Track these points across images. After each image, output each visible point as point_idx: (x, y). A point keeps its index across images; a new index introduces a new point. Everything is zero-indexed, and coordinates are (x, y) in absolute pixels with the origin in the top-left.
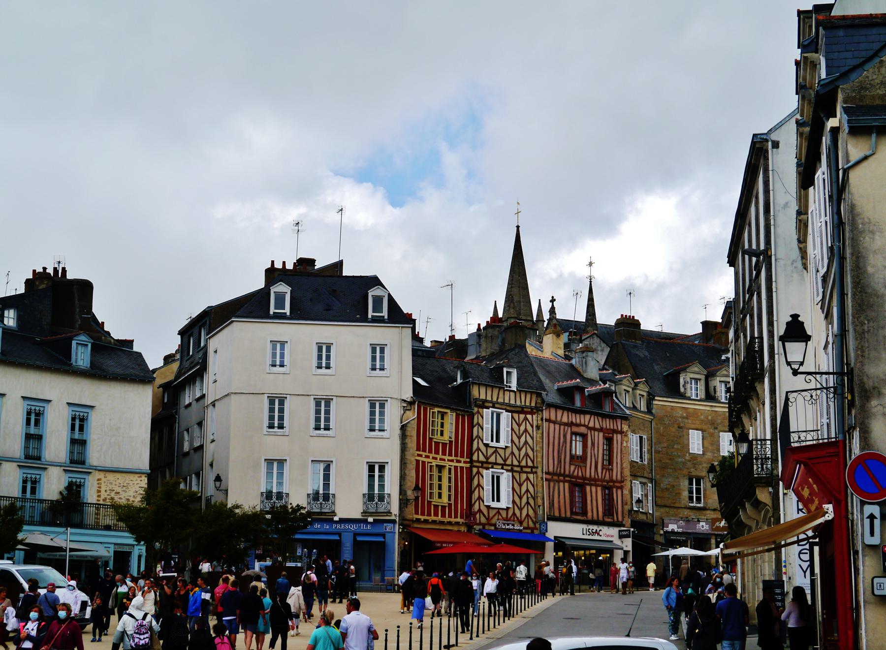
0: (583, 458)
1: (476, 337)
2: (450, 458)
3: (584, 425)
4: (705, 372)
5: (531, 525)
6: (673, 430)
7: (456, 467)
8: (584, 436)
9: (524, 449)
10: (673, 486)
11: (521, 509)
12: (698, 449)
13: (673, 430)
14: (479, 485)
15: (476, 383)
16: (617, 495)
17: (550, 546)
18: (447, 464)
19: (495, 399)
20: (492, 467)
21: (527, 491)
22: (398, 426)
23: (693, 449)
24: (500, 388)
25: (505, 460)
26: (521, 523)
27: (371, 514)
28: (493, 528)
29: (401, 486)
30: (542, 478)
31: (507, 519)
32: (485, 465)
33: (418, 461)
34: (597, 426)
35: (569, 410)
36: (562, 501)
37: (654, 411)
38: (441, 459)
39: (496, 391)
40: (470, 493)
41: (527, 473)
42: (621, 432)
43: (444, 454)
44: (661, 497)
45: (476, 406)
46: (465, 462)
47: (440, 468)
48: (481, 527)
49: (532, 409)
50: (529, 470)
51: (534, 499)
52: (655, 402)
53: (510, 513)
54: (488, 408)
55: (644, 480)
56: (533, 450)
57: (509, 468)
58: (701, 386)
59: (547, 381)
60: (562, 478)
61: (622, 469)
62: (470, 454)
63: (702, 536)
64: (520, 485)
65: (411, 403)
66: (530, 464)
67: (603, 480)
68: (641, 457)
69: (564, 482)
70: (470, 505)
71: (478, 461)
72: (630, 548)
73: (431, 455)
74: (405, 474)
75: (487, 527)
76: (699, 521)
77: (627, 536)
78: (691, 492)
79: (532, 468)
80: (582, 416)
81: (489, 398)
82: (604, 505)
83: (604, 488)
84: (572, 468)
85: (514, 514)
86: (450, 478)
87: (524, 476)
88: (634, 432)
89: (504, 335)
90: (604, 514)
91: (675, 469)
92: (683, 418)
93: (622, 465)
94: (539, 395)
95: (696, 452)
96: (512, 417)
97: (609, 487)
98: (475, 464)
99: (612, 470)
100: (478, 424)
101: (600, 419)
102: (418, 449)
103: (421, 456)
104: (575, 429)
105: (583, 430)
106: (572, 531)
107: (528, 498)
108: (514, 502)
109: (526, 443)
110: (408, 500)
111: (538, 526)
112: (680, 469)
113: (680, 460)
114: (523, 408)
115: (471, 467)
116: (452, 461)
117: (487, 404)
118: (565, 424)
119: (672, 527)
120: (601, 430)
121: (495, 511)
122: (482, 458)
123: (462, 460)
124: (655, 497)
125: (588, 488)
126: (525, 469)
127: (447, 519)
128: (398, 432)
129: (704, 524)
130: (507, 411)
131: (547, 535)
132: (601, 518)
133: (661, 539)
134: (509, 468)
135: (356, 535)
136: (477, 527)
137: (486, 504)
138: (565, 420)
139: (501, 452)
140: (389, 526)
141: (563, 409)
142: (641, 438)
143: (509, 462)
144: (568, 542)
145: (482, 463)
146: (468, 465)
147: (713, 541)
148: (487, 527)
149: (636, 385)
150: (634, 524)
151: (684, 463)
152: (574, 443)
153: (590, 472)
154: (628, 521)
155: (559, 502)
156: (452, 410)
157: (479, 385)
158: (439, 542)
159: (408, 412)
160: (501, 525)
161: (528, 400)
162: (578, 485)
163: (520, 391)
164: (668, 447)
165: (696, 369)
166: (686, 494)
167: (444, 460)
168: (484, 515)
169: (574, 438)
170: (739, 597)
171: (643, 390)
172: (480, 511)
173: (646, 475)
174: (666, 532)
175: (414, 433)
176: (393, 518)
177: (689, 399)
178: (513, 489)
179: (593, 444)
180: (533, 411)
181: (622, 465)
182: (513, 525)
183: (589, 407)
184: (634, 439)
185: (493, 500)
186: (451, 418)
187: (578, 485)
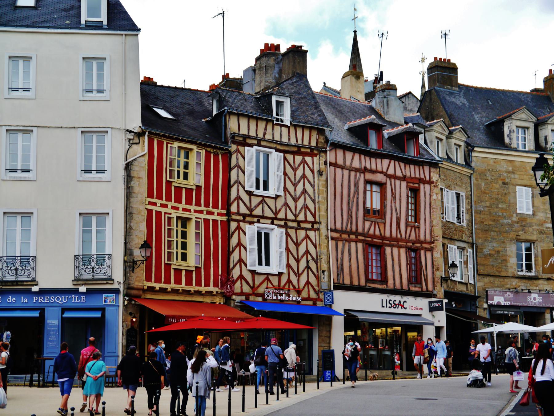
0: (381, 214)
1: (251, 72)
2: (198, 208)
3: (382, 172)
4: (534, 119)
5: (313, 295)
6: (497, 186)
7: (206, 221)
8: (381, 185)
9: (302, 200)
10: (498, 252)
11: (298, 275)
12: (528, 209)
13: (497, 186)
14: (239, 244)
15: (234, 114)
16: (426, 258)
17: (338, 322)
18: (194, 216)
19: (260, 135)
20: (258, 222)
21: (307, 252)
22: (122, 164)
23: (521, 208)
24: (268, 121)
25: (276, 213)
26: (299, 292)
27: (85, 282)
28: (260, 299)
29: (126, 244)
30: (327, 237)
31: (279, 288)
32: (248, 219)
33: (150, 212)
34: (399, 174)
35: (361, 152)
36: (354, 266)
37: (473, 164)
38: (184, 210)
39: (262, 125)
40: (227, 254)
41: (306, 229)
42: (430, 182)
43: (189, 202)
44: (484, 265)
45: (234, 142)
46: (219, 214)
47: (184, 221)
48: (243, 298)
49: (312, 149)
50: (309, 226)
51: (316, 263)
52: (474, 154)
53: (284, 279)
54: (251, 146)
55: (462, 245)
56: (314, 201)
57: (282, 223)
58: (530, 135)
59: (336, 120)
60: (353, 237)
61: (432, 226)
62: (227, 204)
63: (535, 310)
64: (297, 245)
65: (140, 135)
66: (310, 218)
67: (408, 241)
68: (459, 218)
69: (356, 241)
70: (227, 270)
71: (238, 214)
72: (443, 323)
73: (170, 204)
74: (131, 228)
75: (252, 298)
76: (530, 292)
77: (441, 309)
78: (519, 257)
79: (313, 223)
80: (379, 161)
81: (252, 133)
82: (409, 270)
83: (409, 250)
84: (367, 224)
85: (289, 281)
86: (197, 234)
87: (302, 234)
88: (449, 187)
89: (281, 65)
90: (410, 282)
91: (500, 232)
92: (509, 172)
93: (431, 222)
94: (321, 132)
95: (525, 212)
96: (285, 159)
97: (415, 249)
98: (234, 217)
99: (419, 228)
100: (238, 166)
101: (402, 165)
102: (150, 195)
103: (155, 204)
104: (369, 176)
105: (380, 178)
106: (369, 303)
107: (308, 261)
108: (288, 266)
109: (304, 191)
110: (134, 262)
111: (321, 296)
112: (506, 232)
113: (505, 221)
114: (299, 147)
115: (229, 221)
116: (201, 212)
117: (249, 141)
118: (357, 170)
119: (498, 300)
120: (404, 178)
121: (262, 278)
122: (243, 210)
123: (216, 211)
124: (477, 264)
125: (388, 250)
126: (303, 225)
127: (194, 288)
128: (122, 173)
129: (536, 295)
130: (277, 150)
131: (335, 307)
132: (405, 286)
133: (485, 314)
134: (282, 223)
135: (64, 310)
136: (238, 299)
137: (249, 268)
138: (356, 164)
139: (271, 202)
140: (111, 297)
141: (354, 150)
142: (458, 195)
143: (281, 215)
144: (360, 316)
145: (244, 216)
146: (224, 218)
147: (548, 316)
148: (252, 298)
149: (451, 132)
150: (447, 294)
151: (511, 225)
152: (369, 193)
153: (389, 229)
154: (440, 291)
155: (350, 266)
156: (200, 145)
157: (239, 115)
158: (173, 317)
159: (134, 146)
160: (271, 295)
161: (308, 139)
162: (376, 245)
163: (295, 126)
164: (490, 207)
165: (523, 116)
166: (513, 261)
167: (189, 211)
168: (248, 283)
169: (368, 187)
170: (5, 367)
171: (459, 138)
172: (241, 277)
173: (465, 239)
174: (490, 306)
175: (144, 174)
176: (116, 286)
177: (516, 150)
178: (288, 250)
179: (393, 196)
180: (313, 152)
181: (431, 222)
182: (288, 295)
183: (388, 148)
184: (450, 196)
185: (260, 263)
186: (197, 158)
187: (376, 245)
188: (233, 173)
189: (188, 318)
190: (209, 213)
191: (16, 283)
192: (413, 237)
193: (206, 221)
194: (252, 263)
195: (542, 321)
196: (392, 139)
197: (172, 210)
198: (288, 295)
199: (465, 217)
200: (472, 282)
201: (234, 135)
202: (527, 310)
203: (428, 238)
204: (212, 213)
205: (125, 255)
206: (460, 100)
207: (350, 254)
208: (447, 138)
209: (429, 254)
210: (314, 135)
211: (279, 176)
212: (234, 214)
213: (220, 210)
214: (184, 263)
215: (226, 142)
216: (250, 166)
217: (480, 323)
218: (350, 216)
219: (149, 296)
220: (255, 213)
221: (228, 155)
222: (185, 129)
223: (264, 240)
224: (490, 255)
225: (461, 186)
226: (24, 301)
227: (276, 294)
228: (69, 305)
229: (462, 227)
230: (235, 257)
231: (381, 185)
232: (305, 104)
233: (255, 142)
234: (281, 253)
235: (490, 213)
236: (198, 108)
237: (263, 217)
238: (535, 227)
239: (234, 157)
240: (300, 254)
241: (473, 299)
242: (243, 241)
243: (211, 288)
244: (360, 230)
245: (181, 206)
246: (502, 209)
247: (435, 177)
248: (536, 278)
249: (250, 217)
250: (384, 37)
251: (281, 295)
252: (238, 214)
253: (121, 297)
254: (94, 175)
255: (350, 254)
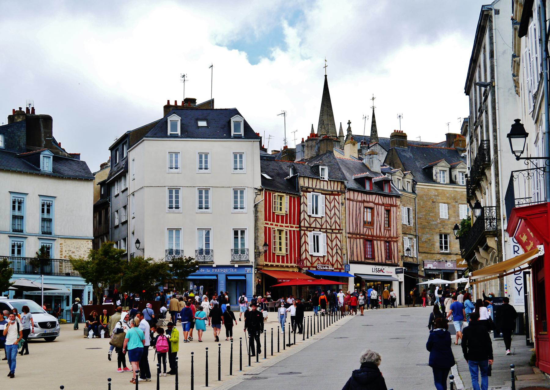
0: (371, 223)
2: (287, 225)
3: (372, 202)
4: (449, 166)
5: (339, 267)
6: (429, 203)
7: (290, 231)
9: (334, 218)
10: (430, 240)
11: (332, 257)
12: (446, 216)
13: (429, 203)
14: (305, 242)
16: (394, 246)
17: (351, 280)
18: (284, 229)
20: (314, 230)
24: (317, 179)
25: (322, 226)
26: (333, 265)
27: (237, 262)
28: (315, 269)
29: (255, 243)
30: (346, 237)
32: (309, 229)
34: (380, 202)
35: (362, 192)
37: (416, 192)
38: (280, 226)
39: (315, 181)
42: (396, 206)
44: (422, 247)
45: (302, 191)
46: (296, 227)
48: (307, 269)
49: (338, 192)
50: (337, 231)
52: (417, 186)
53: (326, 259)
54: (310, 192)
55: (411, 236)
56: (339, 219)
57: (325, 230)
58: (447, 174)
60: (358, 236)
61: (397, 229)
62: (299, 222)
63: (449, 271)
64: (332, 241)
65: (261, 190)
66: (338, 227)
68: (409, 222)
70: (300, 255)
71: (304, 227)
73: (274, 223)
74: (258, 236)
75: (311, 269)
76: (446, 262)
77: (401, 272)
79: (339, 230)
80: (371, 196)
82: (386, 252)
83: (386, 242)
84: (365, 229)
85: (328, 260)
86: (286, 238)
87: (334, 235)
88: (404, 205)
89: (319, 145)
90: (386, 259)
91: (431, 229)
92: (436, 196)
93: (397, 227)
94: (342, 183)
95: (444, 217)
97: (388, 242)
98: (302, 228)
99: (390, 230)
100: (304, 203)
101: (382, 197)
102: (266, 220)
103: (267, 224)
104: (366, 204)
105: (371, 205)
106: (365, 270)
107: (337, 250)
108: (328, 252)
109: (335, 214)
111: (343, 267)
112: (434, 229)
113: (434, 223)
114: (332, 191)
115: (300, 230)
116: (288, 227)
118: (360, 202)
119: (429, 266)
120: (383, 205)
122: (307, 225)
124: (418, 247)
125: (375, 242)
126: (334, 231)
128: (253, 209)
130: (322, 194)
131: (350, 273)
132: (384, 261)
133: (423, 274)
134: (325, 230)
136: (305, 269)
139: (319, 220)
140: (248, 270)
141: (358, 191)
142: (409, 209)
143: (324, 227)
144: (363, 277)
145: (307, 228)
146: (298, 229)
147: (456, 274)
148: (311, 269)
149: (405, 175)
150: (405, 264)
151: (436, 225)
152: (365, 213)
154: (401, 263)
156: (287, 194)
158: (280, 279)
160: (320, 267)
161: (336, 187)
162: (369, 240)
163: (330, 181)
166: (438, 244)
167: (283, 226)
168: (309, 261)
171: (409, 178)
172: (306, 258)
174: (425, 269)
175: (263, 210)
176: (251, 264)
178: (327, 244)
179: (378, 214)
180: (339, 193)
181: (397, 227)
182: (328, 267)
183: (375, 189)
184: (404, 210)
187: (369, 240)
188: (302, 206)
189: (291, 279)
190: (292, 227)
191: (204, 262)
192: (387, 235)
193: (290, 231)
194: (311, 251)
195: (453, 277)
196: (376, 183)
197: (275, 227)
198: (328, 267)
199: (412, 221)
200: (416, 256)
201: (302, 187)
202: (445, 271)
203: (395, 235)
204: (293, 227)
205: (255, 249)
206: (409, 155)
207: (357, 245)
208: (403, 178)
209: (395, 244)
210: (339, 184)
211: (323, 207)
212: (303, 227)
213: (296, 226)
214: (280, 252)
215: (298, 191)
216: (310, 202)
217: (420, 279)
218: (357, 225)
219: (265, 269)
220: (312, 226)
221: (299, 198)
222: (278, 184)
223: (316, 239)
224: (425, 241)
225: (410, 204)
226: (208, 271)
227: (322, 267)
228: (229, 273)
229: (411, 227)
230: (303, 249)
231: (372, 209)
232: (334, 168)
233: (312, 190)
234: (324, 246)
235: (426, 219)
236: (281, 172)
237: (316, 228)
238: (450, 226)
239: (302, 198)
240: (333, 246)
241: (417, 265)
242: (307, 241)
243: (293, 264)
244: (362, 233)
245: (279, 224)
246: (432, 216)
247: (398, 203)
248: (450, 254)
249: (310, 228)
250: (367, 119)
251: (325, 267)
252: (304, 227)
253: (253, 269)
254: (239, 210)
255: (357, 245)
